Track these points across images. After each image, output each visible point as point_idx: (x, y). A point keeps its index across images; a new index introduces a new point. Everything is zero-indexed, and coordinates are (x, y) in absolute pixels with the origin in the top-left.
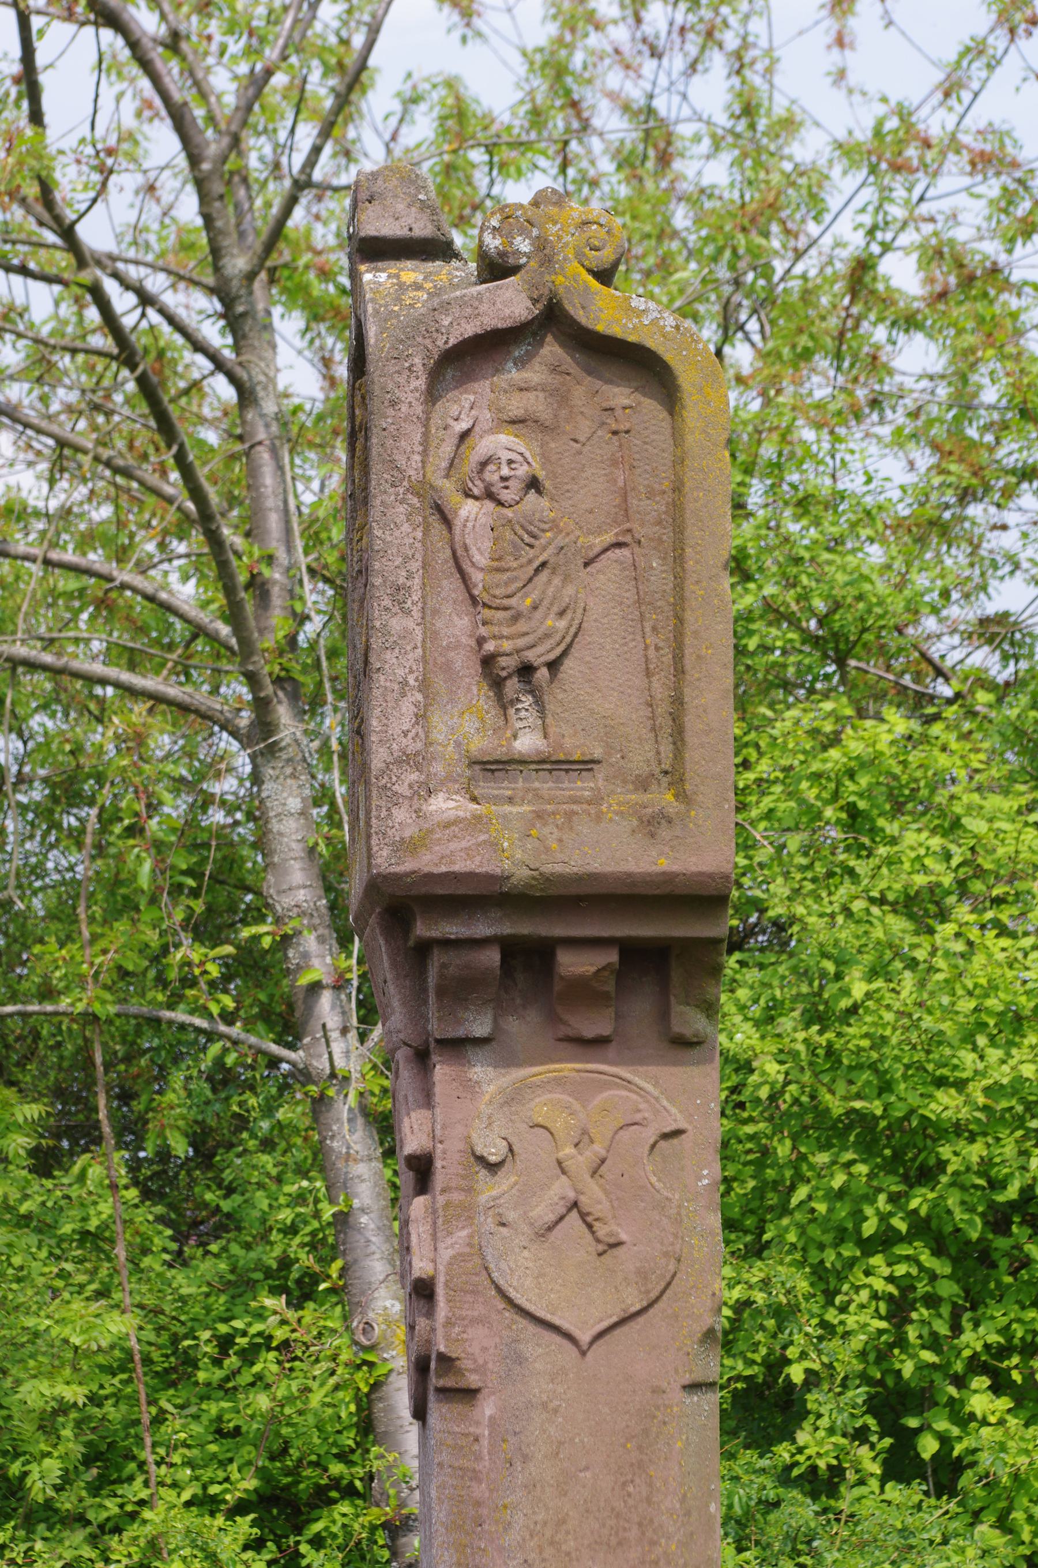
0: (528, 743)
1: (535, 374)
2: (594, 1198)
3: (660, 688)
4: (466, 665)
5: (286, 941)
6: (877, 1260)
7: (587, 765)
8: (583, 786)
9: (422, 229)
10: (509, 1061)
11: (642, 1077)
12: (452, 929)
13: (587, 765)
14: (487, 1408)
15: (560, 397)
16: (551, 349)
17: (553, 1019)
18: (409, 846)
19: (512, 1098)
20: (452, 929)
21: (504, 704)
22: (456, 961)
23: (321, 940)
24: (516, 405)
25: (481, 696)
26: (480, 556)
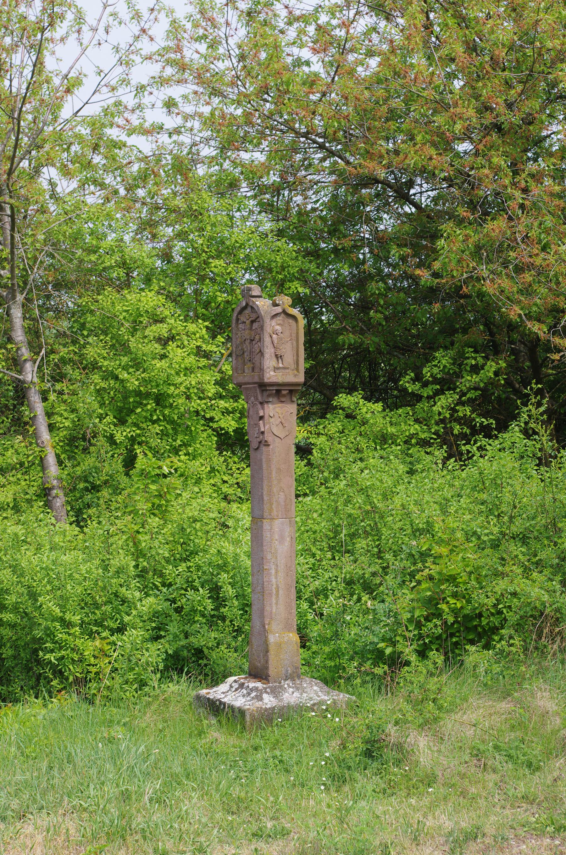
0: (281, 365)
1: (280, 318)
2: (283, 421)
3: (295, 358)
4: (273, 355)
5: (18, 349)
6: (156, 425)
7: (288, 368)
8: (287, 371)
9: (259, 294)
10: (273, 404)
11: (288, 406)
12: (271, 388)
13: (288, 368)
14: (271, 447)
15: (284, 321)
16: (283, 315)
17: (279, 398)
18: (269, 379)
19: (274, 409)
20: (271, 388)
21: (278, 361)
22: (270, 392)
23: (26, 349)
24: (279, 322)
25: (275, 359)
26: (276, 342)
